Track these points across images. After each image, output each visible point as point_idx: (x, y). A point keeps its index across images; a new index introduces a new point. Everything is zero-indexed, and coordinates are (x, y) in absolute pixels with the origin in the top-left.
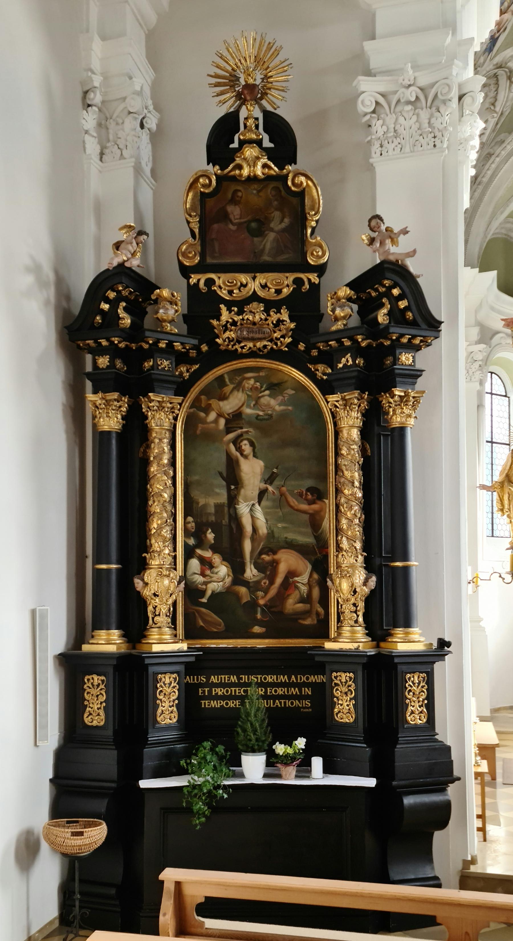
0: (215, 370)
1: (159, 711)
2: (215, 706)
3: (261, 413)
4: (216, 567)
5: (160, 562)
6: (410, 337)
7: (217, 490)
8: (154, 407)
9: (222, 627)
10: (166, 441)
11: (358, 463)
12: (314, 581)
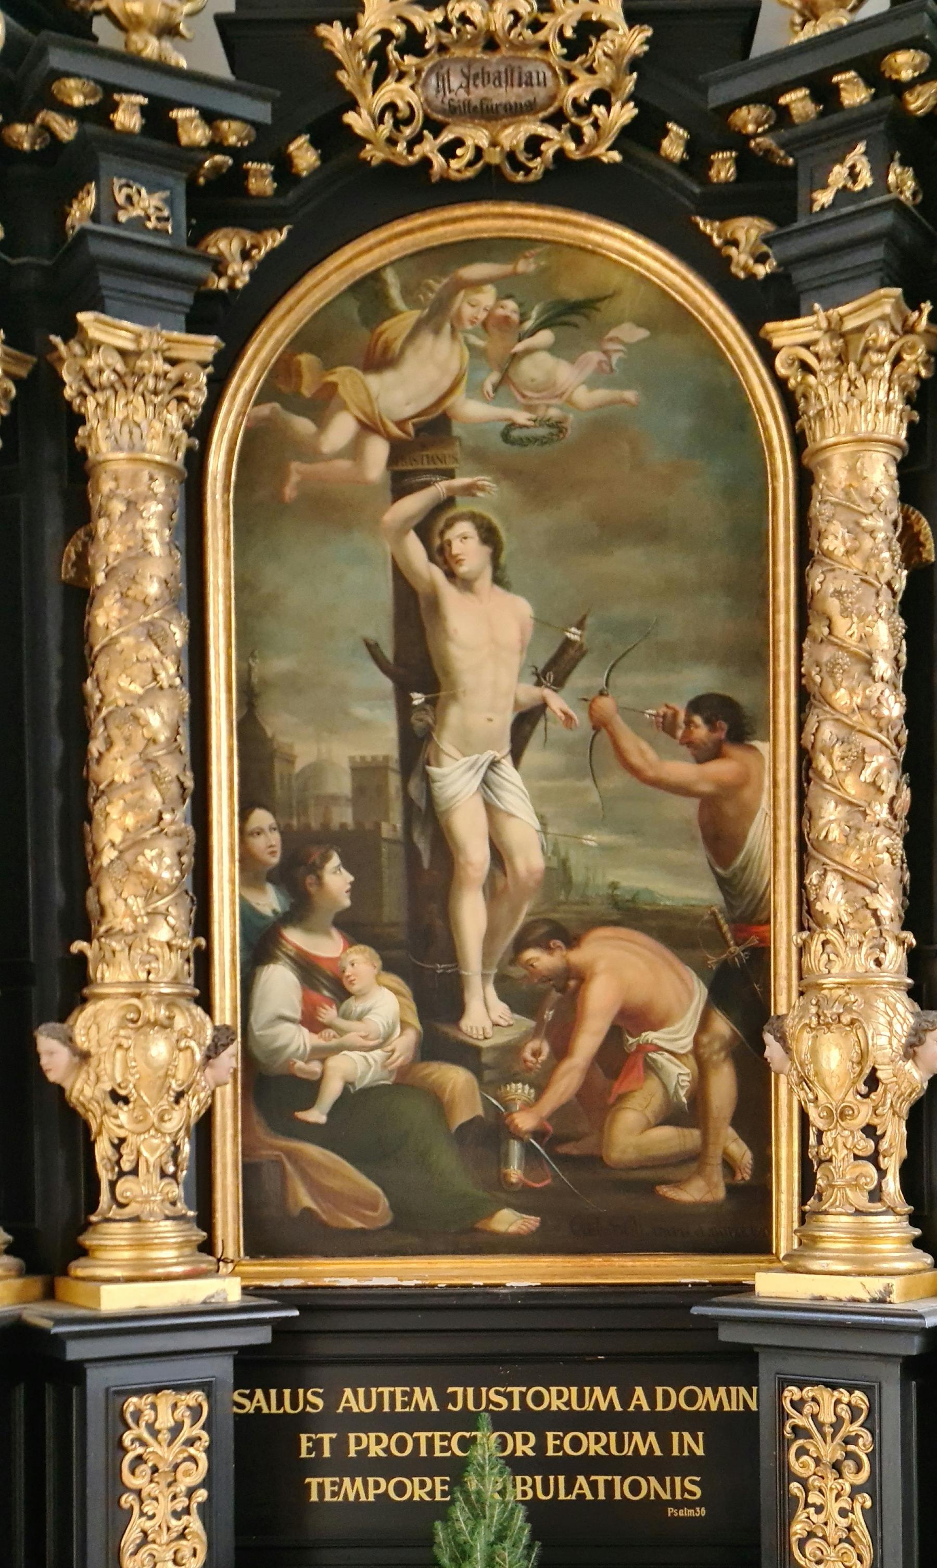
0: (349, 251)
1: (132, 1536)
2: (357, 1495)
3: (522, 417)
4: (360, 996)
5: (135, 972)
7: (361, 711)
8: (100, 371)
9: (382, 1214)
10: (155, 508)
11: (889, 585)
12: (717, 1046)
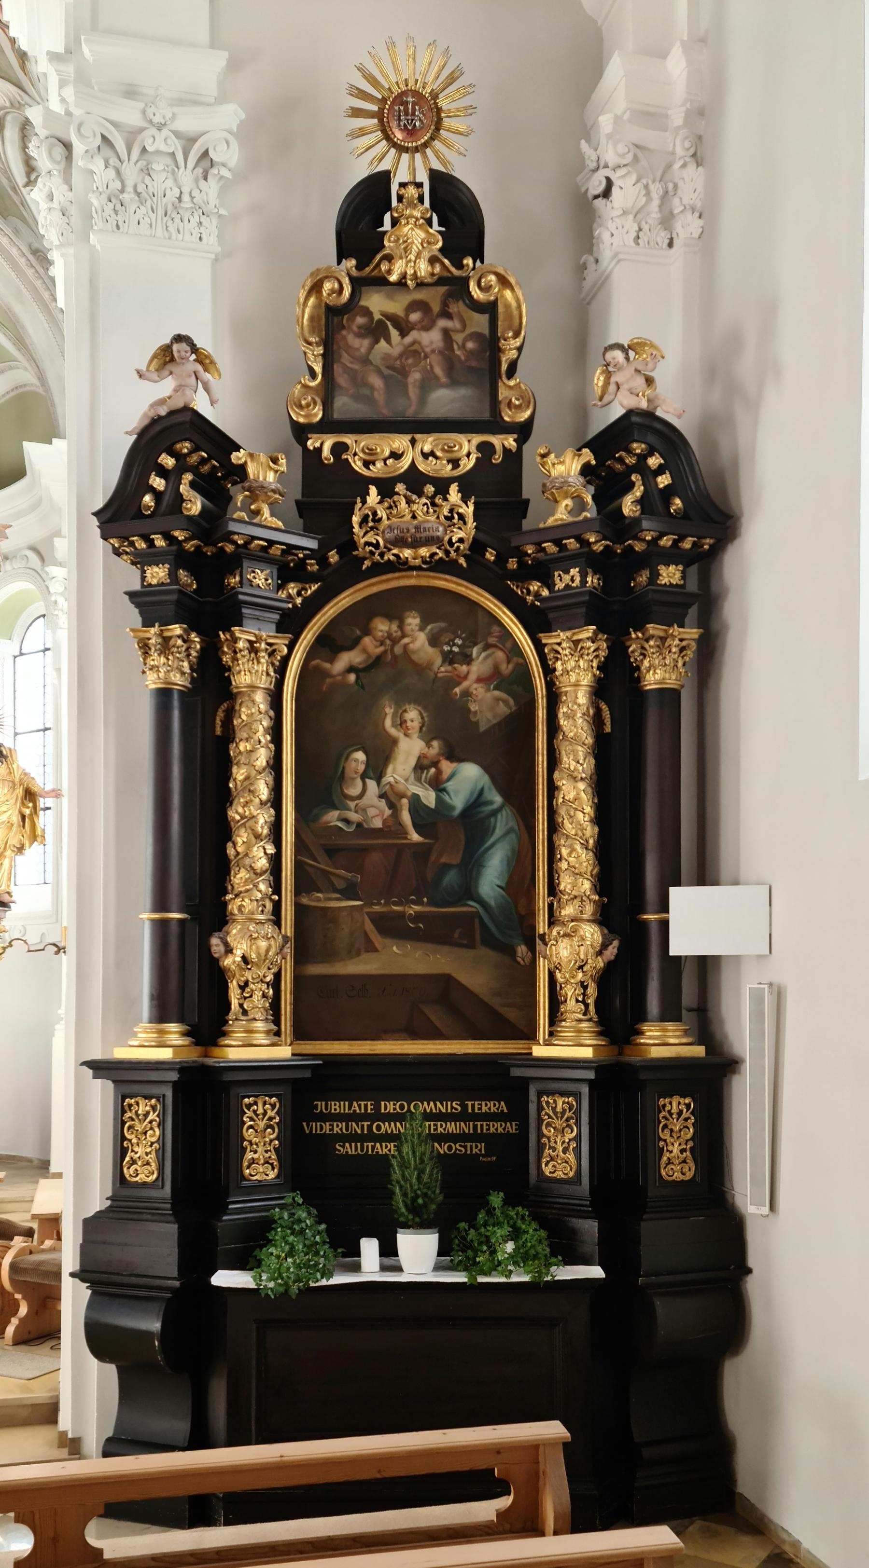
6: (676, 537)
